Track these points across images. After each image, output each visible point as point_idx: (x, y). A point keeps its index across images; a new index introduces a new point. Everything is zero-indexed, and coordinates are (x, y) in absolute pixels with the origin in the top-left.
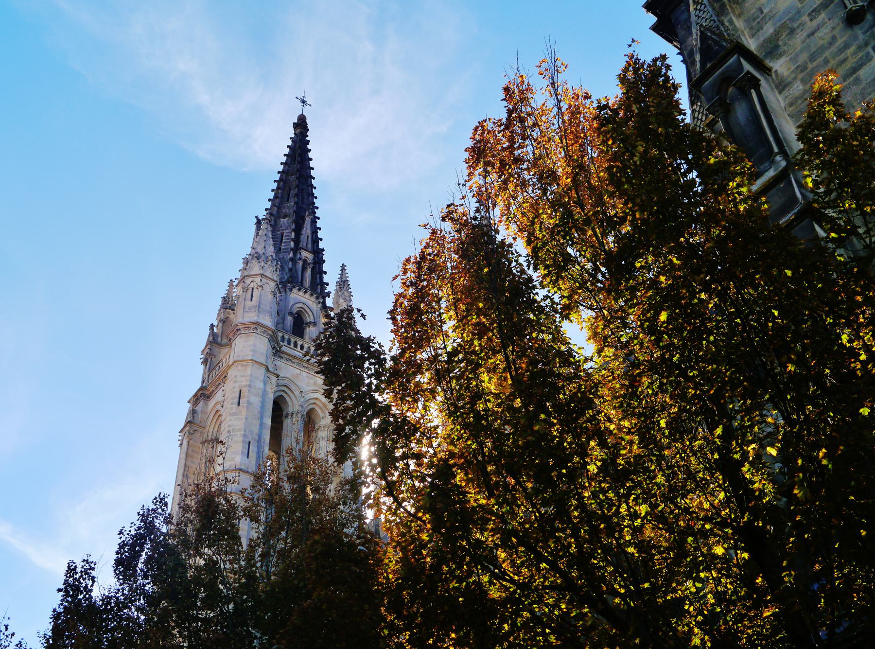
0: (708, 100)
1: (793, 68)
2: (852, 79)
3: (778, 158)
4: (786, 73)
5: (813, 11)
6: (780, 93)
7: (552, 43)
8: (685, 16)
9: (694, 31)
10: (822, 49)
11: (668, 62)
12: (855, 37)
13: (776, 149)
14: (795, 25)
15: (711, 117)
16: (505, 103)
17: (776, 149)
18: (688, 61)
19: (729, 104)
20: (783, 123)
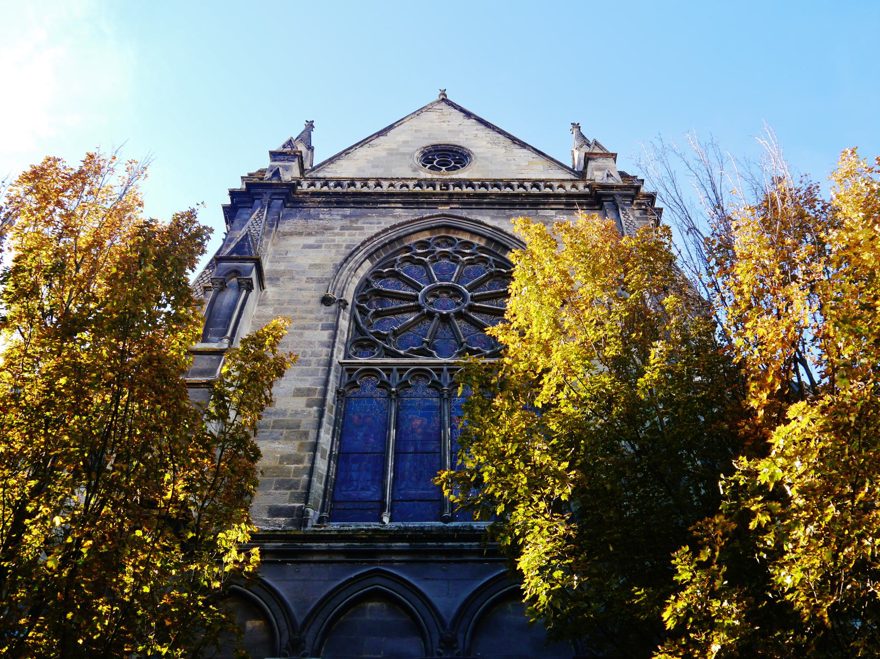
0: (217, 274)
1: (276, 298)
2: (299, 331)
3: (226, 341)
4: (270, 298)
5: (311, 278)
6: (258, 305)
7: (152, 158)
8: (246, 217)
9: (243, 229)
10: (298, 302)
11: (211, 235)
12: (319, 311)
13: (229, 334)
14: (296, 277)
15: (210, 284)
16: (82, 164)
17: (229, 334)
18: (226, 242)
19: (226, 287)
20: (246, 323)
